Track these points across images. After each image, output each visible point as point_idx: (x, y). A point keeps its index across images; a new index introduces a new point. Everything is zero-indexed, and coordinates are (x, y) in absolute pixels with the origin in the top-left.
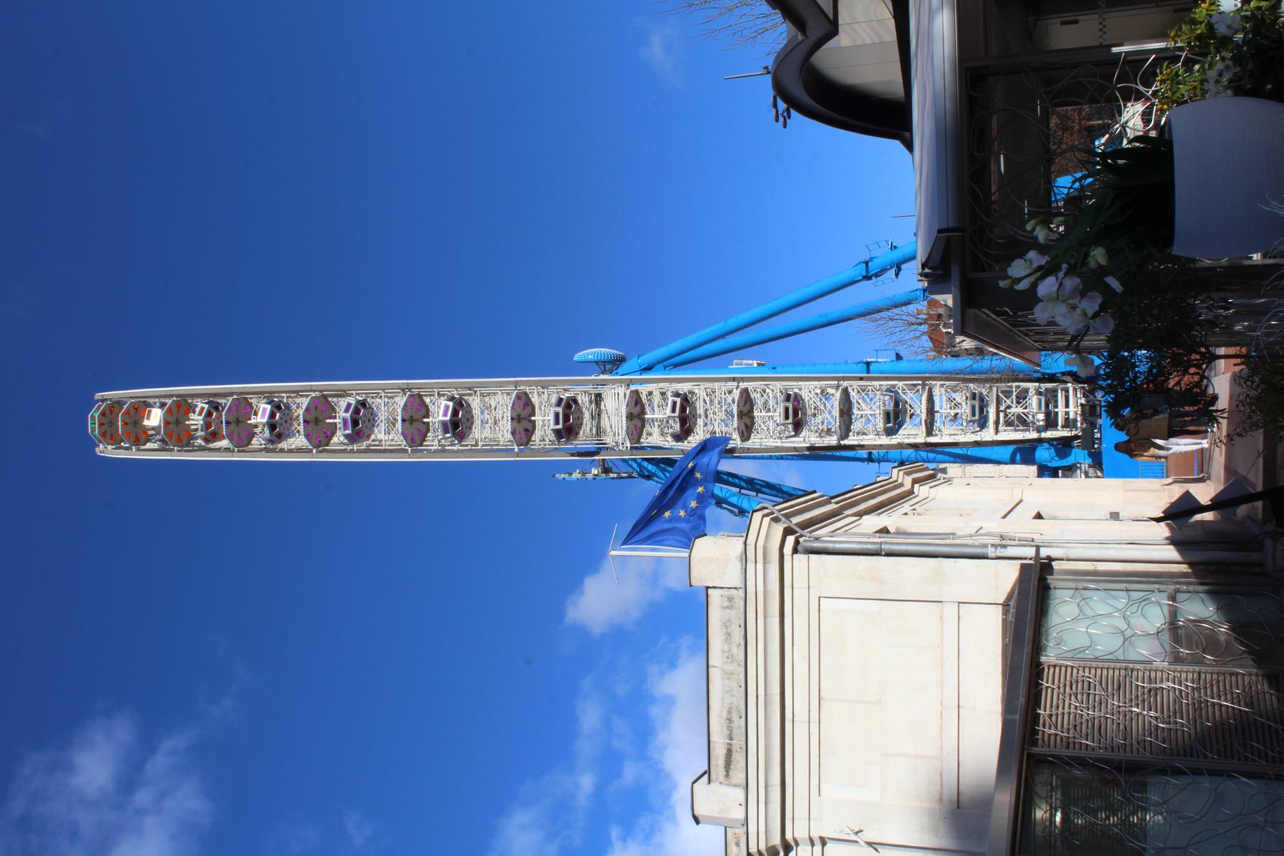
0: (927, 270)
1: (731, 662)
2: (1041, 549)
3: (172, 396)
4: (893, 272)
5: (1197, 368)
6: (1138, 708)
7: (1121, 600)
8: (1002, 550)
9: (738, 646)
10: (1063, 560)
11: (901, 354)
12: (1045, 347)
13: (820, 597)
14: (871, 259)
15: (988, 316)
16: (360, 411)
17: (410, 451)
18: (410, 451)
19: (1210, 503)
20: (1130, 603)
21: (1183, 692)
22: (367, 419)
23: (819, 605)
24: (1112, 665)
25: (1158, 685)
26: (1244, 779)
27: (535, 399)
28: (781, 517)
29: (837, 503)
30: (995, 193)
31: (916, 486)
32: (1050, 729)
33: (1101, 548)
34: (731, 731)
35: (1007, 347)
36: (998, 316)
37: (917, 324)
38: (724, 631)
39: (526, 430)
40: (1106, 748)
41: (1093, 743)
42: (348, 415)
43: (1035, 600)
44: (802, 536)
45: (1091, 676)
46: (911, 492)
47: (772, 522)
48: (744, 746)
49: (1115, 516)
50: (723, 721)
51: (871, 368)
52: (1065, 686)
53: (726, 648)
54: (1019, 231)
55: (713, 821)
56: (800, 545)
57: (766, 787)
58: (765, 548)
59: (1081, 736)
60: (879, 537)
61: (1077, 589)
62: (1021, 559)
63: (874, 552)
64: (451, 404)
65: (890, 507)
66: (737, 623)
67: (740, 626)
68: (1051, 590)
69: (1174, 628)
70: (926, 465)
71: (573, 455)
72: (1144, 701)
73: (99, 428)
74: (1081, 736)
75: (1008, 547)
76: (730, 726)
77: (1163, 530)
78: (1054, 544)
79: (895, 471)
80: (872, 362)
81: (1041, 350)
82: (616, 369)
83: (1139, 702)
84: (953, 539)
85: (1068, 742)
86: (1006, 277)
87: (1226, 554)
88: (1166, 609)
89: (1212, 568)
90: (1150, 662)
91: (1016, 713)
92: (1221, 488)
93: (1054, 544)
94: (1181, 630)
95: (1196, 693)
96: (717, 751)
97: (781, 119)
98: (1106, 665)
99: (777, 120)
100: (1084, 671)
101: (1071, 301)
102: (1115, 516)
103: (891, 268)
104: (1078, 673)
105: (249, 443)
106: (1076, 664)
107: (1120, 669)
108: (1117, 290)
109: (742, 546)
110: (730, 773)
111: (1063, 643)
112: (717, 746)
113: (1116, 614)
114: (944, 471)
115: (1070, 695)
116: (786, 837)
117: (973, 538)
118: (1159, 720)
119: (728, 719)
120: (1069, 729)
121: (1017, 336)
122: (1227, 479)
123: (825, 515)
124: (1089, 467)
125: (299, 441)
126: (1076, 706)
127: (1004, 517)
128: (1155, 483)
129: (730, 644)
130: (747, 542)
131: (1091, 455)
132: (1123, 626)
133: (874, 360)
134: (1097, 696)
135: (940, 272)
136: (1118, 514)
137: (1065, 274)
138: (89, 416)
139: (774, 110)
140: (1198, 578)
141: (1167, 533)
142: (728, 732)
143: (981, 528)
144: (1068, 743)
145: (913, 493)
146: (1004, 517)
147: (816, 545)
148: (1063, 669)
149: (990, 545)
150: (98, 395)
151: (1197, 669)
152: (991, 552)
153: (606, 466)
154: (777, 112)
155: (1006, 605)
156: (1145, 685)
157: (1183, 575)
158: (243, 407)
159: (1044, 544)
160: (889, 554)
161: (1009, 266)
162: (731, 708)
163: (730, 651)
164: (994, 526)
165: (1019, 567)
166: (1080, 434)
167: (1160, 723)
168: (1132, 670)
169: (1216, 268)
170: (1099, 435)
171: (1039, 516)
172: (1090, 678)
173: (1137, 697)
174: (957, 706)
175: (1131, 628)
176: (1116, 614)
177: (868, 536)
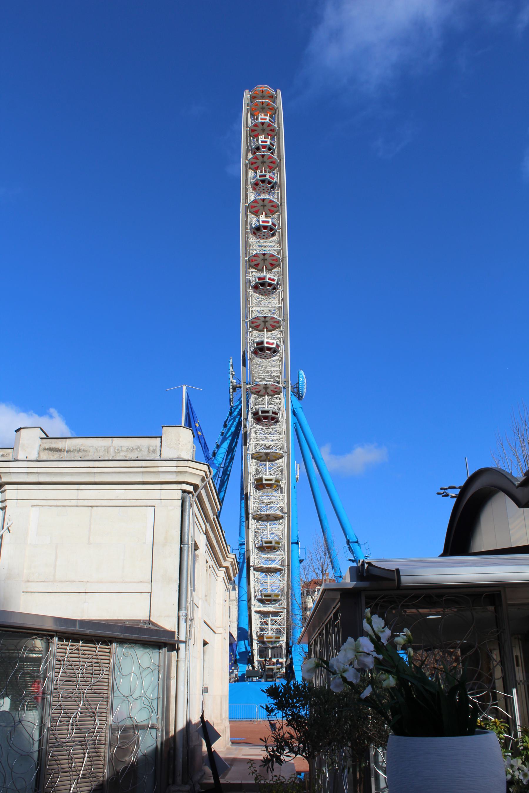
0: (366, 565)
1: (115, 452)
2: (184, 644)
3: (279, 127)
4: (352, 558)
5: (303, 749)
6: (82, 705)
7: (152, 694)
8: (184, 620)
9: (125, 456)
10: (177, 658)
11: (303, 563)
12: (311, 646)
13: (155, 506)
14: (359, 545)
15: (334, 608)
16: (270, 287)
17: (247, 320)
18: (247, 320)
19: (213, 750)
20: (150, 700)
21: (92, 734)
22: (264, 188)
23: (150, 506)
24: (110, 689)
25: (97, 718)
26: (35, 774)
27: (276, 332)
28: (205, 483)
29: (214, 519)
30: (419, 612)
31: (224, 569)
32: (69, 649)
33: (184, 682)
34: (73, 452)
35: (312, 623)
36: (334, 614)
37: (322, 571)
38: (135, 447)
39: (259, 392)
40: (57, 685)
41: (60, 677)
42: (267, 177)
43: (152, 640)
44: (193, 495)
45: (103, 675)
46: (221, 566)
47: (202, 477)
48: (63, 459)
49: (205, 690)
50: (79, 447)
51: (295, 545)
52: (97, 659)
53: (124, 449)
54: (392, 627)
55: (17, 440)
56: (188, 494)
57: (37, 473)
58: (185, 472)
59: (65, 669)
60: (192, 543)
61: (159, 666)
62: (178, 632)
63: (182, 540)
64: (275, 283)
65: (217, 563)
66: (139, 456)
67: (137, 457)
68: (158, 651)
69: (134, 728)
70: (237, 576)
71: (244, 354)
72: (87, 709)
73: (261, 155)
74: (65, 669)
75: (185, 624)
76: (75, 451)
77: (196, 719)
78: (187, 653)
79: (234, 556)
80: (298, 545)
81: (309, 644)
82: (294, 395)
83: (86, 706)
84: (191, 589)
85: (61, 661)
86: (372, 613)
87: (181, 760)
88: (145, 723)
89: (172, 751)
90: (112, 713)
91: (80, 628)
92: (221, 755)
93: (187, 653)
94: (133, 732)
95: (92, 742)
96: (60, 443)
97: (442, 491)
98: (110, 685)
99: (442, 489)
100: (106, 671)
101: (356, 662)
102: (205, 690)
103: (354, 557)
104: (105, 667)
105: (250, 168)
106: (111, 666)
107: (107, 693)
108: (362, 695)
109: (187, 458)
110: (46, 451)
111: (124, 657)
112: (64, 443)
113: (143, 691)
114: (234, 589)
115: (91, 662)
116: (6, 485)
117: (191, 602)
118: (75, 718)
119: (80, 450)
120: (69, 661)
121: (319, 628)
122: (227, 759)
123: (206, 511)
124: (236, 674)
125: (252, 197)
126: (84, 666)
127: (205, 622)
128: (226, 714)
129: (126, 451)
130: (189, 461)
131: (243, 675)
132: (135, 696)
133: (299, 547)
134: (91, 679)
135: (365, 574)
136: (207, 692)
137: (375, 658)
138: (267, 86)
139: (447, 487)
140: (165, 741)
141: (194, 722)
142: (72, 450)
143: (198, 607)
144: (60, 661)
145: (220, 567)
146: (205, 622)
147: (187, 504)
148: (108, 658)
149: (187, 612)
150: (279, 92)
151: (107, 743)
152: (183, 613)
153: (237, 389)
154: (446, 489)
155: (149, 622)
156: (97, 710)
157: (167, 732)
158: (273, 166)
159: (187, 646)
160: (181, 548)
161: (379, 617)
162: (87, 451)
163: (122, 451)
164: (199, 615)
165: (173, 630)
166: (256, 669)
167: (73, 719)
168: (107, 701)
169: (369, 760)
170: (255, 680)
171: (205, 643)
172: (102, 674)
173: (90, 705)
174: (87, 592)
175: (134, 701)
176: (143, 691)
177: (193, 537)
